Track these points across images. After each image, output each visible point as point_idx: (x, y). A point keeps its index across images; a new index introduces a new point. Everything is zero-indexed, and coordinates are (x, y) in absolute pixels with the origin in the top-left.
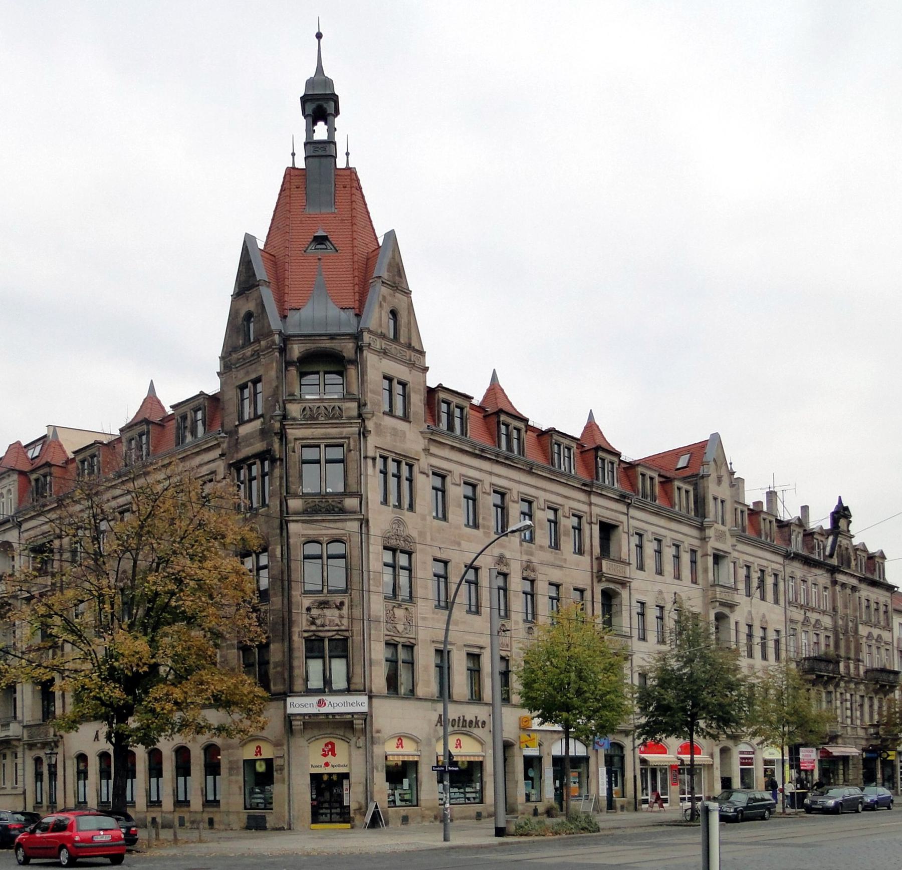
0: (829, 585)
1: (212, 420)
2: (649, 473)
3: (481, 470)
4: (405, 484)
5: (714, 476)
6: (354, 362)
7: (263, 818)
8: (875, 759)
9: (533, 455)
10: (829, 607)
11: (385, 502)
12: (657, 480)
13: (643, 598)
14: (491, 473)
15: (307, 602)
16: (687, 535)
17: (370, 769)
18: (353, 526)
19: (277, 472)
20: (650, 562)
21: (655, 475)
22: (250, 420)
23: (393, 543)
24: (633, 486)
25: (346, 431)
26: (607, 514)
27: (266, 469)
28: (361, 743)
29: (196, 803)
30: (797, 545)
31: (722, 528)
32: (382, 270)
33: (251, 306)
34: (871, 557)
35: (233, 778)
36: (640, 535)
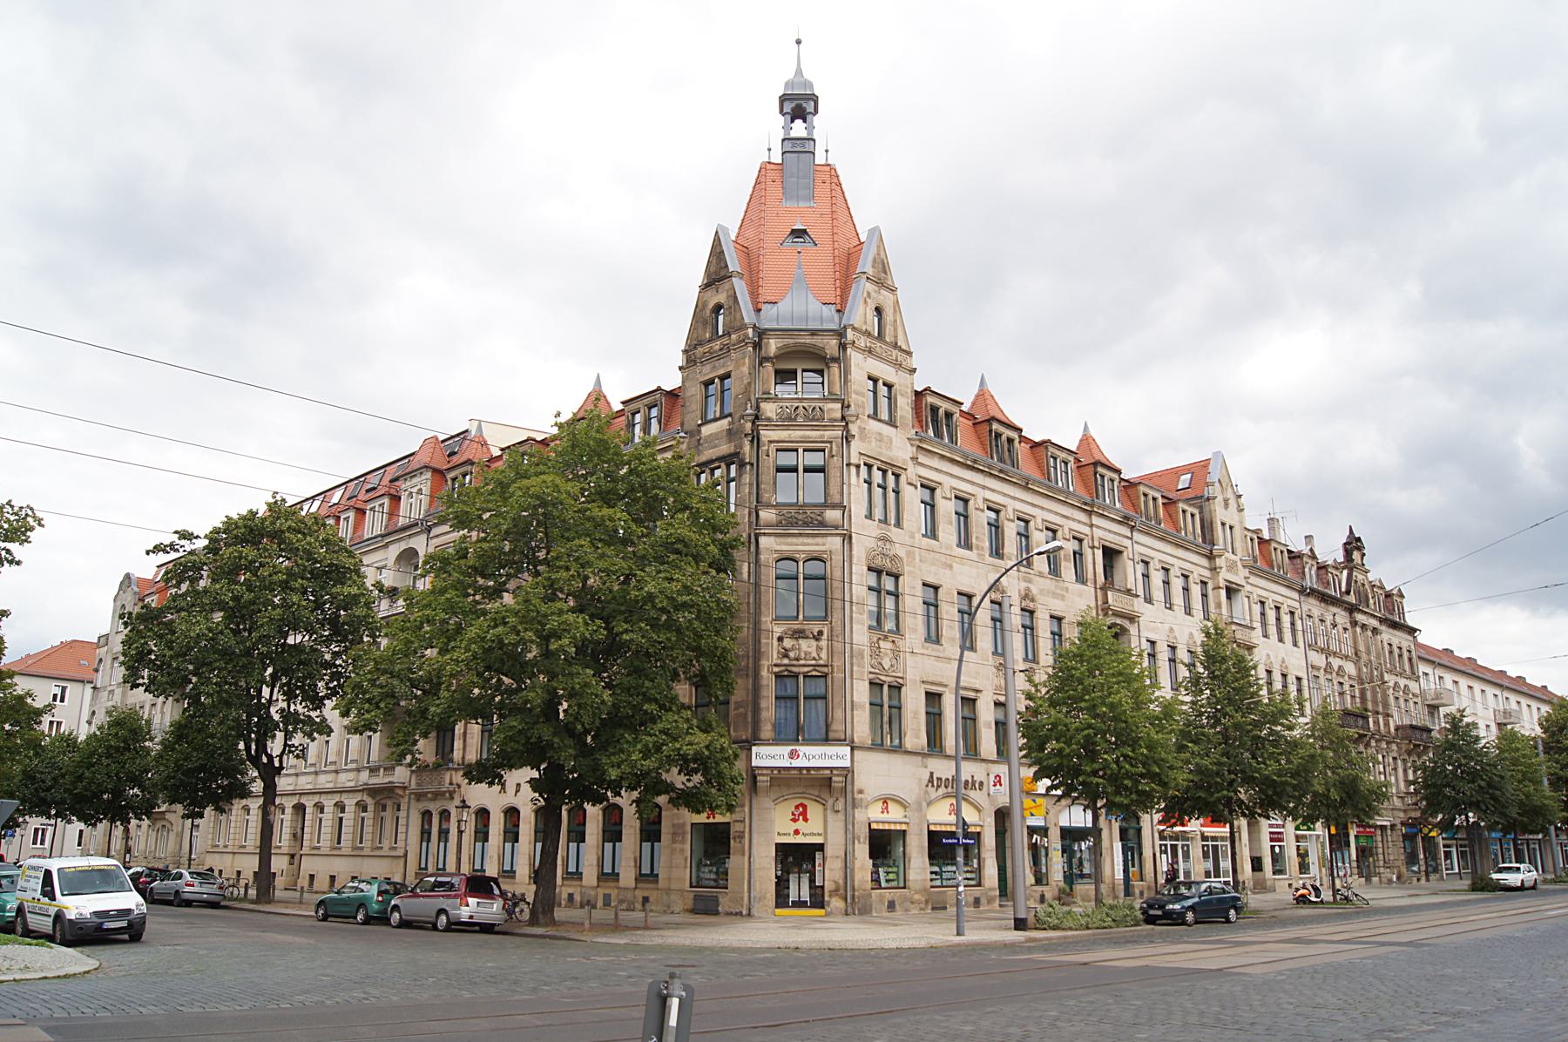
0: (1348, 626)
1: (669, 418)
2: (1152, 493)
3: (973, 483)
4: (891, 495)
5: (1220, 499)
6: (836, 360)
7: (716, 900)
8: (1415, 835)
9: (1027, 467)
10: (1351, 652)
11: (870, 516)
12: (1160, 501)
13: (1153, 637)
14: (984, 487)
15: (778, 630)
16: (1197, 566)
17: (850, 839)
18: (834, 543)
19: (747, 478)
20: (1158, 594)
21: (1158, 495)
22: (715, 420)
23: (878, 562)
24: (1135, 506)
25: (827, 434)
26: (1111, 537)
27: (733, 474)
28: (840, 806)
29: (627, 876)
30: (1311, 580)
31: (1233, 557)
32: (866, 265)
33: (721, 298)
34: (1388, 595)
35: (678, 846)
36: (1147, 563)
